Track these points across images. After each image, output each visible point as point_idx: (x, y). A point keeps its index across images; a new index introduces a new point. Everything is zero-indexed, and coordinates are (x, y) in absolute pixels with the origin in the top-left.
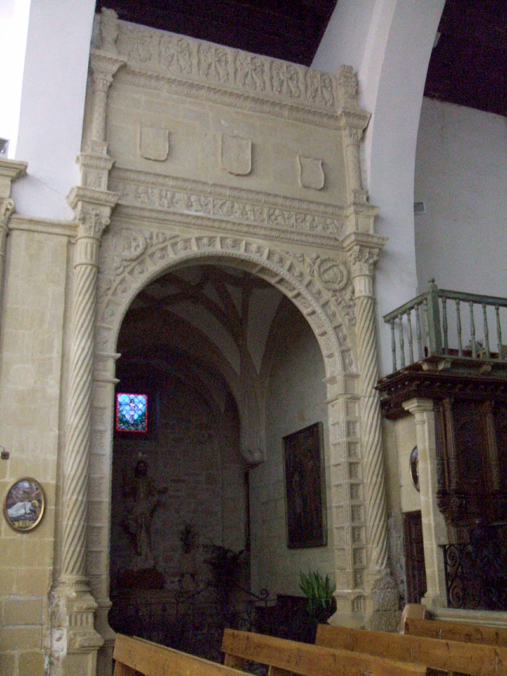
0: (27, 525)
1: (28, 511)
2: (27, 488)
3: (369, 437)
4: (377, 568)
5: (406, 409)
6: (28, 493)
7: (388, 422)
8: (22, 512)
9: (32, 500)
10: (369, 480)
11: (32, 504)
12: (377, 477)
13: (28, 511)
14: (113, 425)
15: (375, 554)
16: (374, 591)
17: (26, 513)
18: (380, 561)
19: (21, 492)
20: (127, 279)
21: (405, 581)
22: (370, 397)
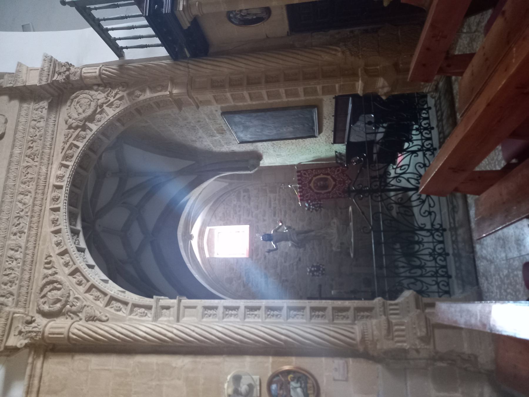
0: (311, 385)
1: (299, 385)
2: (277, 386)
3: (225, 67)
4: (339, 54)
5: (189, 25)
6: (282, 385)
7: (211, 50)
8: (299, 390)
9: (288, 380)
10: (261, 65)
11: (293, 380)
12: (260, 58)
13: (299, 385)
14: (141, 304)
15: (327, 58)
16: (360, 56)
17: (301, 387)
18: (333, 52)
19: (281, 392)
20: (327, 310)
21: (352, 29)
22: (188, 68)
